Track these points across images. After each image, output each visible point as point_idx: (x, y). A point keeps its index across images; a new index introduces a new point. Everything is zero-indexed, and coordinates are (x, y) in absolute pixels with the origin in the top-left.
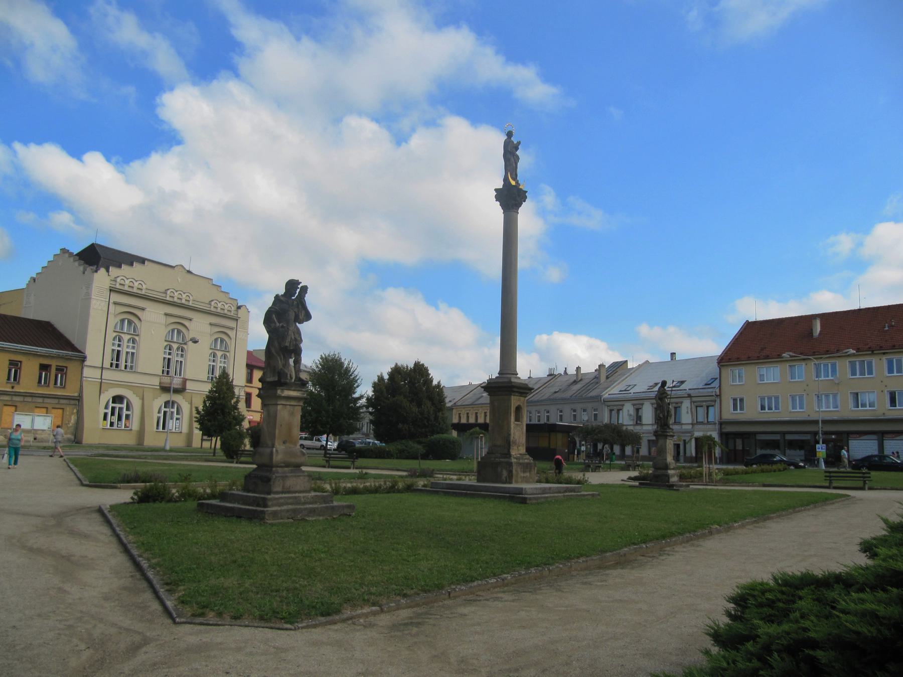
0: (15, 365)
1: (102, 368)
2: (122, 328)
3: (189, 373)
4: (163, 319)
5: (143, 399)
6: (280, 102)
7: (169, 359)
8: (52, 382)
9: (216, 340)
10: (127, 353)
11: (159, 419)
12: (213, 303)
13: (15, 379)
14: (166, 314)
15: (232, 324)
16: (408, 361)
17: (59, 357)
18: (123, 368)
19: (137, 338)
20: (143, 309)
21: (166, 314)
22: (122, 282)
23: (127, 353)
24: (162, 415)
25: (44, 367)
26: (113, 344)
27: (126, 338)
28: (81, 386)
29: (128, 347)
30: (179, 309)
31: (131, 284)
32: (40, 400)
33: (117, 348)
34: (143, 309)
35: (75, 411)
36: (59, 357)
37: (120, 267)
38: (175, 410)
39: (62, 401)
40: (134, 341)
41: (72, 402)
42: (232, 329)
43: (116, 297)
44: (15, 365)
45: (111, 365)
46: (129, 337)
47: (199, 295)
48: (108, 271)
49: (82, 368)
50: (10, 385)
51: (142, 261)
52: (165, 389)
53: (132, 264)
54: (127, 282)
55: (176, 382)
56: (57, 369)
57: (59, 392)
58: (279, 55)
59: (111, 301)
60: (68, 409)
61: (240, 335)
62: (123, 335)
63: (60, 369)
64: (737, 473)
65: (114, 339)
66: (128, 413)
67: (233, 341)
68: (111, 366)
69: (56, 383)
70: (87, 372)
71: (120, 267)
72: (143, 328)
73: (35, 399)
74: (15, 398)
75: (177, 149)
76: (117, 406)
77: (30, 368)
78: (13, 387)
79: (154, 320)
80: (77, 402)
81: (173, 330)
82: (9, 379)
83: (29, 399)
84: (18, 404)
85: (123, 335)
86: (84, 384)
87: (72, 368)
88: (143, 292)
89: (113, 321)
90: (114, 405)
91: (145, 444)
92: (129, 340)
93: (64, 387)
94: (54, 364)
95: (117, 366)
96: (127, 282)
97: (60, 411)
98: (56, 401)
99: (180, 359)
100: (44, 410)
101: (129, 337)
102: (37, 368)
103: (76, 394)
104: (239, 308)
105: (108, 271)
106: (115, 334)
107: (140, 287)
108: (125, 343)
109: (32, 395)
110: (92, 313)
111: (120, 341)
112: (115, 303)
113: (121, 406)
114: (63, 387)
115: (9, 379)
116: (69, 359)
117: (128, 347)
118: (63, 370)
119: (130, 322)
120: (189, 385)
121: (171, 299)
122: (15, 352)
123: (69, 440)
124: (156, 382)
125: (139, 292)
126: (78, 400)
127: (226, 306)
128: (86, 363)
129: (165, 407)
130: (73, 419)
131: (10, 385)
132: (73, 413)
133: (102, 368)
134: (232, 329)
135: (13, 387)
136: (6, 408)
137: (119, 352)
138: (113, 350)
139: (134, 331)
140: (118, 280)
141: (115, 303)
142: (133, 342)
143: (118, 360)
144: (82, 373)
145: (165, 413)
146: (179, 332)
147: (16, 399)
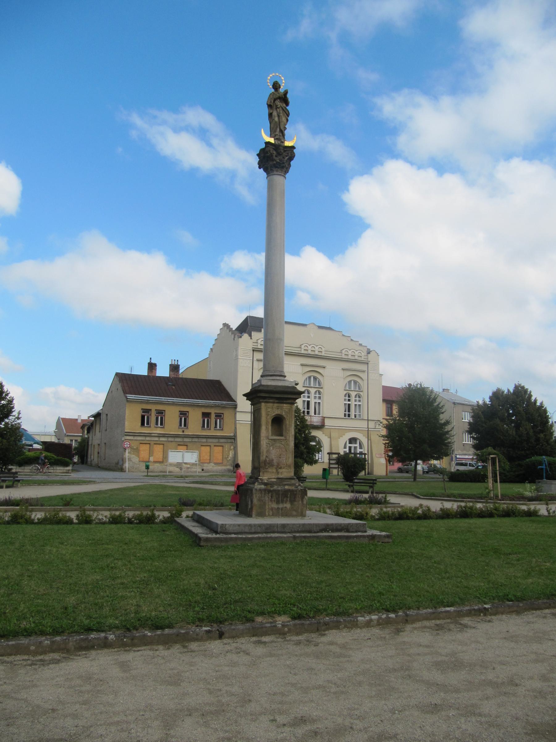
0: (184, 414)
1: (368, 420)
2: (350, 387)
3: (326, 411)
4: (342, 374)
5: (330, 438)
6: (441, 165)
7: (349, 405)
8: (213, 425)
9: (350, 382)
10: (356, 405)
13: (185, 425)
14: (302, 365)
15: (364, 367)
16: (508, 387)
18: (353, 417)
19: (361, 393)
21: (343, 369)
23: (356, 405)
25: (206, 415)
26: (345, 400)
27: (353, 394)
28: (236, 428)
29: (355, 401)
31: (353, 354)
32: (204, 440)
35: (232, 447)
38: (358, 445)
39: (222, 440)
40: (320, 393)
41: (229, 440)
42: (364, 371)
44: (184, 414)
46: (356, 393)
47: (328, 344)
48: (250, 336)
49: (235, 414)
50: (181, 430)
54: (350, 352)
56: (216, 416)
57: (219, 434)
58: (432, 122)
59: (255, 359)
60: (227, 446)
61: (372, 376)
62: (351, 392)
63: (219, 416)
65: (345, 396)
67: (366, 382)
68: (345, 416)
69: (216, 427)
70: (239, 416)
72: (326, 383)
73: (200, 440)
74: (186, 440)
75: (367, 235)
76: (353, 445)
77: (195, 417)
78: (183, 432)
80: (233, 440)
81: (310, 377)
82: (181, 425)
83: (196, 440)
84: (188, 444)
85: (351, 392)
86: (238, 426)
87: (227, 414)
90: (350, 445)
91: (375, 473)
92: (316, 392)
93: (222, 430)
94: (213, 411)
95: (349, 415)
96: (350, 352)
97: (220, 448)
98: (216, 440)
99: (317, 401)
100: (185, 447)
101: (356, 393)
102: (178, 413)
103: (232, 435)
104: (369, 352)
105: (250, 336)
107: (360, 355)
108: (353, 398)
109: (198, 437)
110: (240, 370)
111: (349, 396)
113: (356, 445)
114: (222, 429)
115: (181, 425)
116: (224, 407)
117: (355, 401)
118: (186, 414)
119: (355, 382)
120: (327, 422)
121: (346, 357)
122: (148, 402)
123: (229, 471)
126: (233, 439)
127: (357, 353)
128: (238, 409)
129: (350, 443)
130: (231, 454)
131: (181, 430)
132: (231, 449)
133: (368, 420)
134: (364, 371)
135: (183, 432)
136: (203, 448)
137: (349, 405)
139: (359, 388)
140: (303, 346)
142: (359, 397)
144: (235, 418)
146: (315, 378)
147: (186, 440)
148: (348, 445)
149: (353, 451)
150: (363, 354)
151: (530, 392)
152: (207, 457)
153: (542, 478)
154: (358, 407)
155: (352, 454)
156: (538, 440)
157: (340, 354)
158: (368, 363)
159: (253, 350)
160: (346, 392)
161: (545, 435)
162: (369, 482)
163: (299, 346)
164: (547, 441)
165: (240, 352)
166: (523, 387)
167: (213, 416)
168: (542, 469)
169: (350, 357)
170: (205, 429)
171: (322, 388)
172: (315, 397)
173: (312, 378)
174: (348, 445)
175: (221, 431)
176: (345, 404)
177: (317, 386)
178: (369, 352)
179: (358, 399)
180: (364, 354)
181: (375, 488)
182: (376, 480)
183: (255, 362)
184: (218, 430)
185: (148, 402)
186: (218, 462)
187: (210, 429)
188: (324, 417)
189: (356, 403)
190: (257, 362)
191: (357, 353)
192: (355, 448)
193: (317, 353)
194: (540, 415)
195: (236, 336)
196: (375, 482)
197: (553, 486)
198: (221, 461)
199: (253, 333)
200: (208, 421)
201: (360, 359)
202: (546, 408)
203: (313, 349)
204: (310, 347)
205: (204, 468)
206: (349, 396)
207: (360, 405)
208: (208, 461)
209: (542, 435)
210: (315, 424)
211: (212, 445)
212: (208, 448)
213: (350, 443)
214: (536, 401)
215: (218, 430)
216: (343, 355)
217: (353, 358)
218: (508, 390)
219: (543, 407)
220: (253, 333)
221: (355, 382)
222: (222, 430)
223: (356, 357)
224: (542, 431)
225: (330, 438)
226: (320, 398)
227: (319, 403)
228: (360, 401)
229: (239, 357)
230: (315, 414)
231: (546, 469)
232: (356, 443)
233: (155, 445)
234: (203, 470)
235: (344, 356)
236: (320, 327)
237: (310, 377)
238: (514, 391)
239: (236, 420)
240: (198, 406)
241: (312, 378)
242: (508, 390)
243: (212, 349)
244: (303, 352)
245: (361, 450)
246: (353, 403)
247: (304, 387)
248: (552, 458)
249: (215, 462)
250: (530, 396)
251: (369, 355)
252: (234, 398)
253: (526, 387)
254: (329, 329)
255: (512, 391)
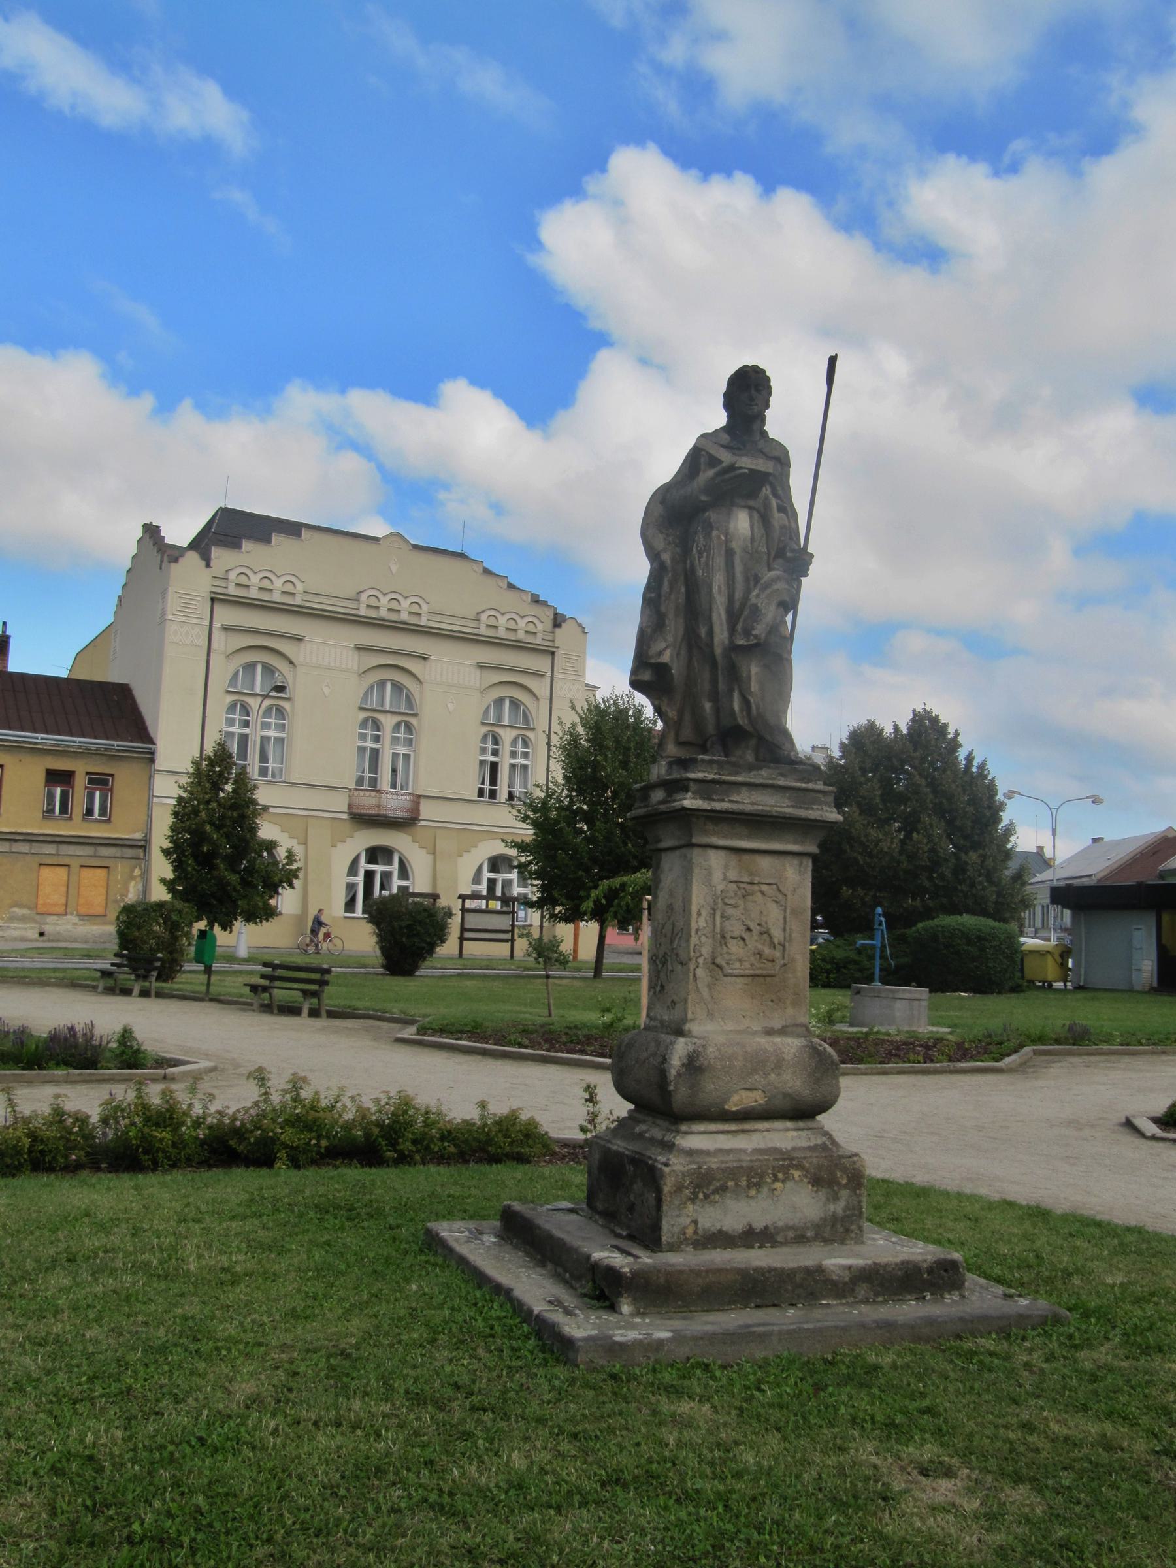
2: (499, 717)
4: (352, 661)
5: (434, 853)
9: (499, 702)
10: (513, 766)
11: (351, 887)
12: (484, 617)
15: (541, 663)
16: (892, 716)
17: (88, 753)
19: (531, 735)
20: (299, 639)
21: (359, 648)
22: (492, 621)
23: (395, 755)
24: (360, 880)
25: (57, 777)
27: (507, 736)
28: (150, 817)
29: (513, 754)
30: (393, 639)
31: (512, 625)
32: (50, 849)
33: (369, 744)
34: (299, 639)
35: (137, 872)
36: (88, 753)
37: (238, 546)
38: (394, 868)
40: (409, 728)
41: (129, 852)
42: (540, 675)
43: (225, 616)
45: (481, 793)
46: (515, 733)
49: (151, 777)
51: (293, 529)
52: (363, 820)
53: (267, 540)
54: (503, 620)
55: (394, 804)
56: (91, 781)
59: (216, 624)
60: (120, 868)
62: (500, 731)
64: (759, 1325)
66: (351, 880)
69: (89, 811)
71: (238, 546)
72: (300, 683)
73: (36, 848)
76: (379, 868)
79: (328, 666)
80: (140, 852)
81: (382, 684)
83: (24, 848)
85: (500, 731)
87: (125, 777)
88: (298, 601)
89: (222, 672)
90: (493, 875)
92: (398, 724)
93: (109, 821)
94: (81, 769)
95: (493, 794)
96: (503, 620)
97: (101, 873)
98: (89, 850)
99: (403, 750)
101: (515, 733)
102: (41, 777)
103: (138, 835)
106: (484, 729)
107: (531, 628)
108: (506, 747)
109: (30, 838)
112: (226, 629)
113: (387, 868)
117: (513, 754)
118: (106, 782)
119: (515, 704)
120: (427, 811)
121: (491, 632)
122: (65, 753)
124: (340, 803)
125: (288, 600)
129: (372, 859)
132: (132, 878)
134: (540, 675)
136: (46, 872)
137: (494, 766)
138: (362, 750)
140: (232, 576)
141: (226, 629)
143: (494, 781)
144: (150, 787)
145: (369, 875)
148: (486, 875)
149: (499, 893)
150: (540, 626)
151: (957, 734)
152: (58, 898)
153: (869, 979)
154: (518, 771)
155: (497, 899)
156: (960, 869)
157: (474, 624)
158: (553, 653)
159: (213, 600)
160: (484, 729)
161: (984, 858)
162: (303, 975)
163: (353, 594)
164: (990, 876)
165: (173, 603)
166: (935, 720)
167: (80, 781)
168: (873, 947)
169: (502, 633)
170: (55, 819)
171: (416, 715)
172: (395, 741)
173: (389, 686)
174: (363, 866)
175: (103, 826)
176: (482, 763)
177: (403, 710)
178: (558, 621)
179: (520, 749)
180: (543, 625)
181: (325, 995)
182: (328, 971)
183: (216, 634)
184: (96, 820)
185: (65, 753)
186: (91, 912)
187: (70, 818)
188: (420, 797)
189: (513, 761)
190: (223, 635)
191: (522, 623)
192: (386, 876)
193: (404, 616)
194: (973, 801)
195: (166, 559)
196: (327, 977)
197: (898, 1005)
198: (99, 910)
199: (215, 552)
200: (64, 795)
201: (530, 639)
202: (993, 780)
203: (394, 605)
204: (384, 601)
205: (47, 929)
206: (496, 741)
207: (525, 767)
208: (61, 910)
209: (973, 856)
210: (391, 814)
211: (75, 864)
212: (62, 872)
213: (372, 859)
214: (970, 759)
215: (96, 820)
216: (483, 626)
217: (511, 636)
218: (896, 728)
219: (986, 777)
220: (215, 552)
221: (515, 704)
222: (109, 821)
223: (521, 635)
224: (976, 846)
225: (434, 853)
226: (409, 742)
227: (407, 757)
228: (525, 755)
229: (169, 617)
230: (394, 786)
231: (883, 946)
232: (390, 863)
233: (85, 871)
234: (42, 934)
235: (483, 630)
236: (415, 547)
237: (382, 684)
238: (910, 728)
239: (151, 796)
240: (34, 750)
241: (389, 686)
242: (896, 728)
243: (120, 599)
244: (363, 611)
245: (404, 883)
246: (505, 761)
247: (361, 709)
248: (991, 922)
249: (83, 911)
250: (954, 745)
251: (557, 630)
252: (152, 735)
253: (943, 720)
254: (461, 556)
255: (905, 731)
